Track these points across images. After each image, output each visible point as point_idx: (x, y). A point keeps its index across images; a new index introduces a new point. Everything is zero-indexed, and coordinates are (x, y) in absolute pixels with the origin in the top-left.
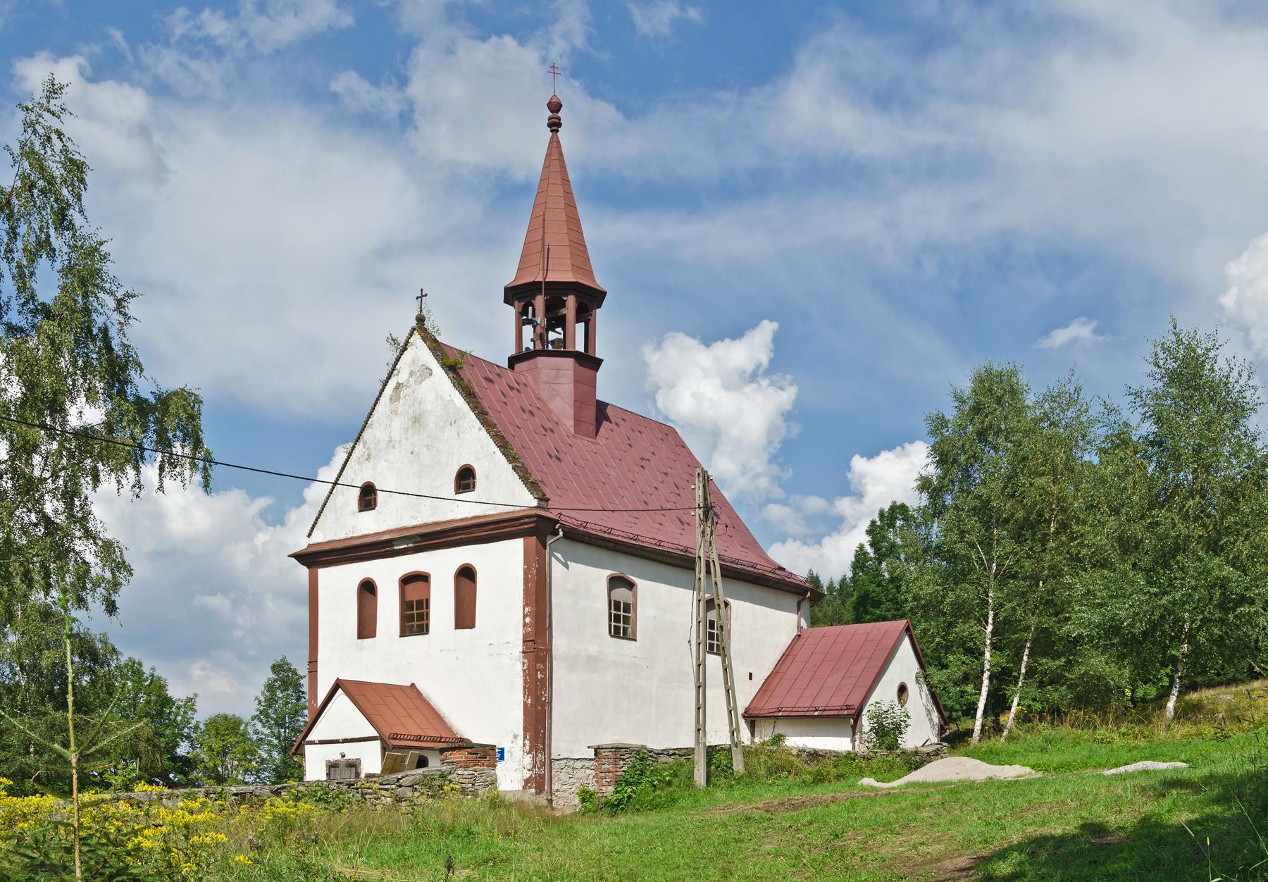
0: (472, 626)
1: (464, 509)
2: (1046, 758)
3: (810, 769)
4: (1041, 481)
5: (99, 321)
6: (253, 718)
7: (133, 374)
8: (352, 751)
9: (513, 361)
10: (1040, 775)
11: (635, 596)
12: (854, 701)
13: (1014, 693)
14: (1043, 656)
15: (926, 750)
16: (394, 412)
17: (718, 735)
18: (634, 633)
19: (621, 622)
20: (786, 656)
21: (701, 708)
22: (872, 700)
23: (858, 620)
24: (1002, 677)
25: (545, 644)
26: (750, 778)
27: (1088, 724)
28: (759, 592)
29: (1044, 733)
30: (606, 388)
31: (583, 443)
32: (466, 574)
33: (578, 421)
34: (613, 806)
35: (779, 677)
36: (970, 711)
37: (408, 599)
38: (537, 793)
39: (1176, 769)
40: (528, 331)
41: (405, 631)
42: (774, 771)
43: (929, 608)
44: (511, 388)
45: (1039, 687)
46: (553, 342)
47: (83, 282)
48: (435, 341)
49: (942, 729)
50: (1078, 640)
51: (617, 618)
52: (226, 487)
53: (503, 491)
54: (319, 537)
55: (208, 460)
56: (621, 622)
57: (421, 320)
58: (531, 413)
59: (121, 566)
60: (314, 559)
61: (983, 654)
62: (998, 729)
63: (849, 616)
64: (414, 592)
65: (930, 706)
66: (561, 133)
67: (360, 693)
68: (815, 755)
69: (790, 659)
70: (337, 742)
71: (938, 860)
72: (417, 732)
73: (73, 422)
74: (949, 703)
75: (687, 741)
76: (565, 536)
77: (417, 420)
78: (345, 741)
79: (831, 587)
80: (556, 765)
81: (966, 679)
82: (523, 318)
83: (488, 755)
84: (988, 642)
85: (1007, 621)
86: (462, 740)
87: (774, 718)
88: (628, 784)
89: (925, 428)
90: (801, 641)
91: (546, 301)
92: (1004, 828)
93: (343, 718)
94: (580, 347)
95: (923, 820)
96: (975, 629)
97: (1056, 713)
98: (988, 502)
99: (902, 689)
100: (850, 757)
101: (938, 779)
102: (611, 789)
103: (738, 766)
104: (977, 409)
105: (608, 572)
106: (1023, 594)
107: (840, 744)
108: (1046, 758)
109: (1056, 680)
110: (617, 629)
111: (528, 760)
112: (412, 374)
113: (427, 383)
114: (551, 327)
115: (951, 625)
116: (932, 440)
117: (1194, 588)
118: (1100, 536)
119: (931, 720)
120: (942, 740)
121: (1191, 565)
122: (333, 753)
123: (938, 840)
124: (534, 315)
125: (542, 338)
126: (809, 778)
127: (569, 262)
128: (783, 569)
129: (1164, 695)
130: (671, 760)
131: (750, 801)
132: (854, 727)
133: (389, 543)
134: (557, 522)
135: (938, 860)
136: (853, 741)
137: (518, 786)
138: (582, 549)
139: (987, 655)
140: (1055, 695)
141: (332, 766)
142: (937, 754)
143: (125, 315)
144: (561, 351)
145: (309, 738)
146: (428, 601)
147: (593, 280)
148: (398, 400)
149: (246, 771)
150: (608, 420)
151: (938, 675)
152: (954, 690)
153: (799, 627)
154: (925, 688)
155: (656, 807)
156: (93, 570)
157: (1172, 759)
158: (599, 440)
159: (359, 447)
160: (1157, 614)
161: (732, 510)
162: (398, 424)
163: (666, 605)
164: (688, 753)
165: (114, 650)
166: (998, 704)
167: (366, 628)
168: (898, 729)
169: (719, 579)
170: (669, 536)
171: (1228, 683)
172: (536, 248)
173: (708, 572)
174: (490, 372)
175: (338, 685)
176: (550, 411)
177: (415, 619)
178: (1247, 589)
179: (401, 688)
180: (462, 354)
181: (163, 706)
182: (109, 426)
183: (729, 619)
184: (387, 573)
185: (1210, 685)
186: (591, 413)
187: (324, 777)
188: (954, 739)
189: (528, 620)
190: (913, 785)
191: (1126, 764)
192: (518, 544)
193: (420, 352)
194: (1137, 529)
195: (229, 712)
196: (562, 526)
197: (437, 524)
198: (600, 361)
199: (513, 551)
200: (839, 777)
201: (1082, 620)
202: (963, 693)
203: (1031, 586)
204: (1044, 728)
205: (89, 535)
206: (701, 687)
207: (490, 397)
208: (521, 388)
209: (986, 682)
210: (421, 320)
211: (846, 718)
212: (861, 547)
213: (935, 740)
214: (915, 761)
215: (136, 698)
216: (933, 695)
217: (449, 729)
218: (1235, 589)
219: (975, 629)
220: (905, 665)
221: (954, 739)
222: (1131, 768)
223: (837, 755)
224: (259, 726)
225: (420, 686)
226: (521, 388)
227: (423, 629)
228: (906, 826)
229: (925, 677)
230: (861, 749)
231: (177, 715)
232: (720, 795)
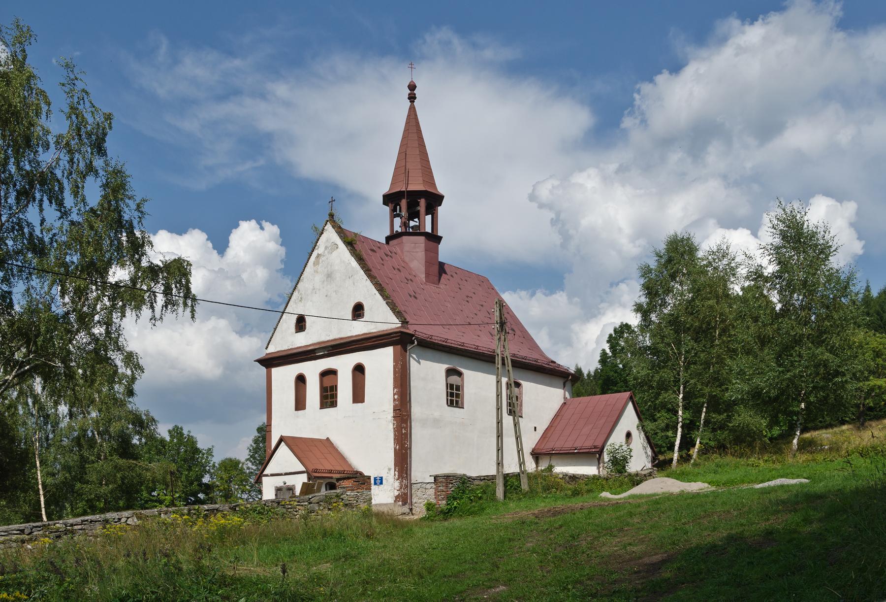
0: (362, 401)
1: (358, 329)
2: (718, 477)
3: (570, 486)
4: (711, 302)
5: (126, 217)
6: (247, 460)
7: (147, 248)
8: (290, 481)
9: (388, 239)
10: (714, 488)
11: (463, 380)
12: (599, 443)
13: (697, 436)
14: (714, 412)
15: (643, 473)
16: (316, 272)
17: (510, 466)
18: (463, 403)
19: (455, 397)
20: (557, 416)
21: (500, 449)
22: (608, 443)
23: (604, 392)
24: (690, 426)
25: (407, 411)
26: (532, 493)
27: (741, 456)
28: (540, 377)
29: (716, 461)
30: (444, 253)
31: (431, 288)
32: (359, 369)
33: (427, 275)
34: (445, 513)
35: (552, 429)
36: (671, 448)
37: (325, 385)
38: (403, 505)
39: (802, 485)
40: (397, 221)
41: (323, 406)
42: (547, 489)
43: (644, 384)
44: (387, 255)
45: (712, 432)
46: (412, 227)
47: (115, 191)
48: (340, 227)
49: (654, 459)
50: (735, 403)
51: (452, 395)
52: (207, 318)
53: (381, 318)
54: (272, 349)
55: (194, 299)
56: (455, 397)
57: (331, 216)
58: (399, 270)
59: (138, 367)
60: (270, 362)
61: (677, 412)
62: (689, 457)
63: (599, 391)
64: (328, 381)
65: (646, 444)
66: (416, 103)
67: (294, 444)
68: (574, 478)
69: (559, 418)
70: (281, 475)
71: (640, 558)
72: (329, 467)
73: (112, 279)
74: (660, 443)
75: (493, 472)
76: (418, 345)
77: (329, 276)
78: (286, 474)
79: (589, 375)
80: (414, 487)
81: (667, 428)
82: (394, 214)
83: (362, 481)
84: (681, 404)
85: (689, 393)
86: (357, 472)
87: (550, 455)
88: (455, 499)
89: (636, 273)
90: (566, 407)
91: (408, 203)
92: (686, 533)
93: (284, 460)
94: (428, 229)
95: (633, 525)
96: (672, 396)
97: (722, 448)
98: (677, 317)
99: (629, 435)
100: (595, 478)
101: (649, 492)
102: (444, 502)
103: (525, 486)
104: (670, 260)
105: (446, 366)
106: (700, 374)
107: (589, 470)
108: (718, 477)
109: (722, 427)
110: (452, 401)
111: (397, 484)
112: (326, 248)
113: (335, 253)
114: (411, 218)
115: (659, 394)
116: (642, 281)
117: (807, 367)
118: (745, 334)
119: (646, 453)
120: (653, 466)
121: (804, 352)
122: (279, 481)
123: (642, 541)
124: (400, 211)
125: (405, 225)
126: (570, 492)
127: (421, 179)
128: (554, 362)
129: (790, 434)
130: (482, 483)
131: (530, 509)
132: (599, 459)
133: (313, 351)
134: (413, 335)
135: (640, 558)
136: (599, 468)
137: (391, 500)
138: (429, 353)
139: (680, 413)
140: (722, 435)
141: (278, 490)
142: (650, 475)
143: (142, 212)
144: (417, 232)
145: (265, 473)
146: (336, 386)
147: (433, 184)
148: (318, 264)
149: (242, 492)
150: (446, 273)
151: (650, 426)
152: (660, 434)
153: (565, 398)
154: (643, 433)
155: (472, 513)
156: (120, 371)
157: (798, 477)
158: (442, 286)
159: (296, 294)
160: (785, 384)
161: (523, 327)
162: (318, 278)
163: (479, 384)
164: (492, 478)
165: (153, 419)
166: (687, 443)
167: (300, 404)
168: (625, 460)
169: (510, 368)
170: (485, 342)
171: (826, 427)
172: (401, 170)
173: (503, 364)
174: (374, 246)
175: (281, 440)
176: (411, 269)
177: (329, 398)
178: (839, 366)
179: (320, 440)
180: (356, 234)
181: (194, 453)
182: (134, 280)
183: (521, 393)
184: (312, 369)
185: (816, 429)
186: (435, 269)
187: (273, 497)
188: (661, 465)
189: (396, 397)
190: (633, 496)
191: (768, 480)
192: (390, 350)
193: (330, 235)
194: (769, 331)
195: (233, 457)
196: (417, 338)
197: (341, 339)
198: (441, 238)
199: (385, 357)
200: (589, 491)
201: (737, 389)
202: (667, 437)
203: (704, 369)
204: (716, 458)
205: (119, 349)
206: (500, 436)
207: (373, 260)
208: (393, 255)
209: (680, 430)
210: (331, 216)
211: (594, 454)
212: (604, 350)
213: (649, 465)
214: (636, 480)
215: (178, 450)
216: (648, 438)
217: (350, 466)
218: (833, 367)
219: (672, 396)
220: (629, 419)
221: (661, 465)
222: (772, 483)
223: (587, 477)
224: (250, 465)
225: (332, 439)
226: (393, 255)
227: (334, 404)
228: (621, 530)
229: (642, 427)
230: (604, 473)
231: (202, 458)
232: (512, 505)
